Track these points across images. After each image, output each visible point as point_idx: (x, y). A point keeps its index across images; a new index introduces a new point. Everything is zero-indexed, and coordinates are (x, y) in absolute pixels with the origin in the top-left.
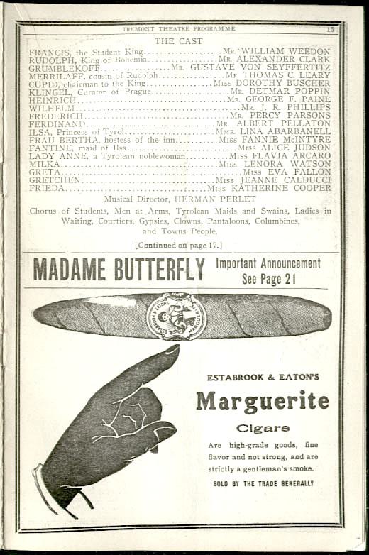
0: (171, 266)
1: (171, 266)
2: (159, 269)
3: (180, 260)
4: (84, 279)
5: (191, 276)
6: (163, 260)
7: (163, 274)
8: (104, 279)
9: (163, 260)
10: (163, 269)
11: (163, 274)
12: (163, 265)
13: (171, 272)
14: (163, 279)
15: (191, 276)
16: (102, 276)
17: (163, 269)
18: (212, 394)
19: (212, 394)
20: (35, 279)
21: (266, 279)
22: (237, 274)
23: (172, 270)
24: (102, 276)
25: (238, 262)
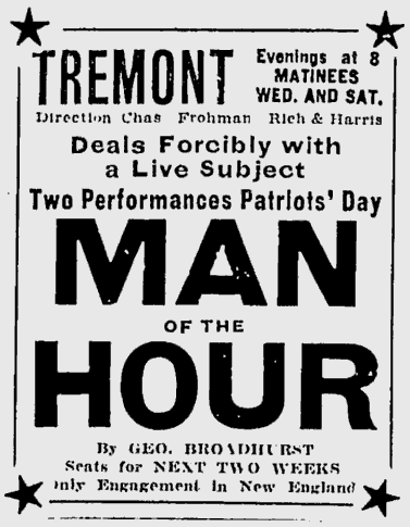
0: (71, 70)
1: (71, 70)
2: (94, 77)
3: (93, 55)
4: (186, 207)
5: (140, 170)
6: (103, 54)
7: (104, 88)
8: (202, 322)
9: (103, 54)
10: (103, 77)
11: (104, 88)
12: (105, 65)
13: (70, 84)
14: (145, 174)
15: (140, 170)
16: (97, 95)
17: (103, 77)
18: (286, 70)
19: (286, 70)
20: (283, 453)
21: (254, 200)
22: (98, 162)
23: (72, 77)
24: (97, 95)
25: (111, 198)
